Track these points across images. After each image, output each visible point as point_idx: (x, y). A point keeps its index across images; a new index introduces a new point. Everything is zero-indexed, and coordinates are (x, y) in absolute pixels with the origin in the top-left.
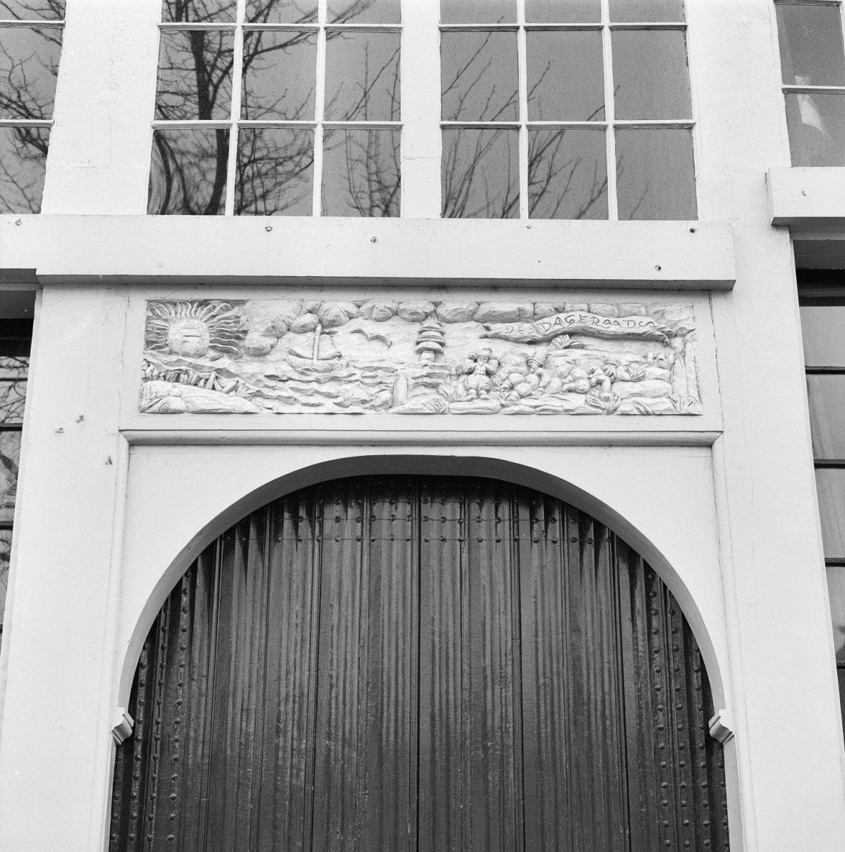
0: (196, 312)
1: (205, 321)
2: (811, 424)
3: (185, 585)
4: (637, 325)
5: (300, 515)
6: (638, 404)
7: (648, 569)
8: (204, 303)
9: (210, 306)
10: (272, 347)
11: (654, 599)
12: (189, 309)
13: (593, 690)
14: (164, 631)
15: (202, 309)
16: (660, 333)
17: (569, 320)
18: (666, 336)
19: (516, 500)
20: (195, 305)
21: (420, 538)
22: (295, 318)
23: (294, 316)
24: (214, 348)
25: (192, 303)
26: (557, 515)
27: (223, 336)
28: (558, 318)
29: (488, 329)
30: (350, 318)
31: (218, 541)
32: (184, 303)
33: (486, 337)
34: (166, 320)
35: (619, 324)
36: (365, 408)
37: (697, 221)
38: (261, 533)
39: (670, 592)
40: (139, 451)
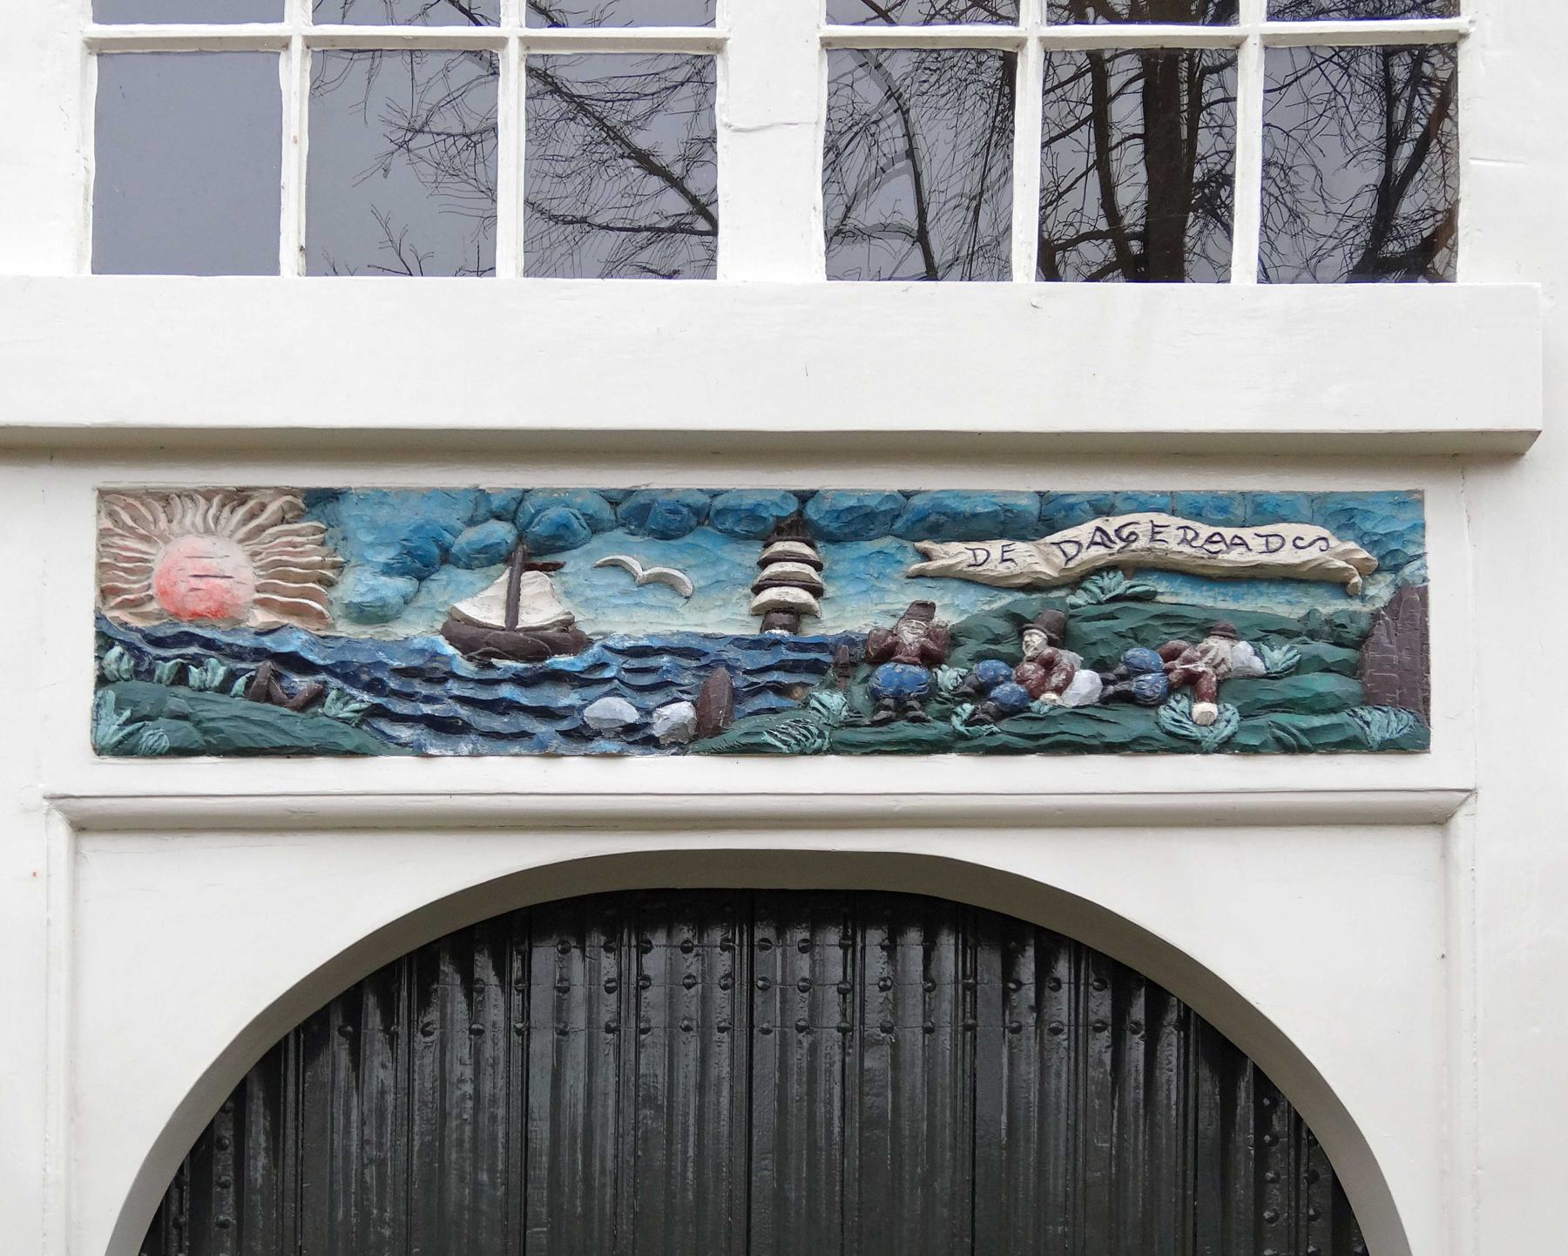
0: (217, 519)
1: (241, 541)
2: (1301, 522)
3: (227, 1134)
4: (1289, 545)
5: (476, 976)
6: (1283, 729)
7: (1263, 1084)
8: (239, 496)
9: (251, 503)
10: (407, 601)
11: (1274, 1149)
12: (201, 512)
13: (968, 1047)
14: (179, 1227)
15: (232, 512)
16: (1341, 564)
17: (1125, 532)
18: (1356, 572)
19: (971, 941)
20: (216, 501)
21: (751, 1026)
22: (460, 532)
23: (458, 525)
24: (263, 603)
25: (208, 495)
26: (1062, 969)
27: (285, 577)
28: (1098, 529)
29: (926, 556)
30: (594, 532)
31: (292, 1046)
32: (188, 495)
33: (920, 575)
34: (146, 539)
35: (1244, 544)
36: (629, 743)
37: (821, 34)
38: (389, 1016)
39: (1309, 1132)
40: (91, 843)
